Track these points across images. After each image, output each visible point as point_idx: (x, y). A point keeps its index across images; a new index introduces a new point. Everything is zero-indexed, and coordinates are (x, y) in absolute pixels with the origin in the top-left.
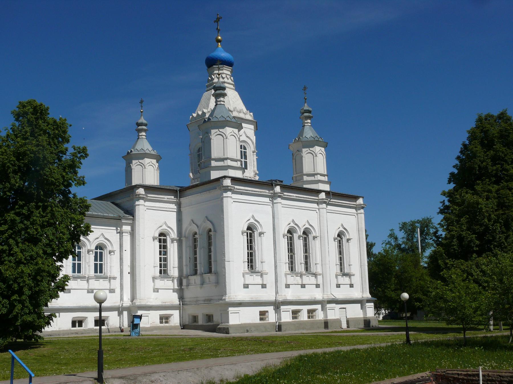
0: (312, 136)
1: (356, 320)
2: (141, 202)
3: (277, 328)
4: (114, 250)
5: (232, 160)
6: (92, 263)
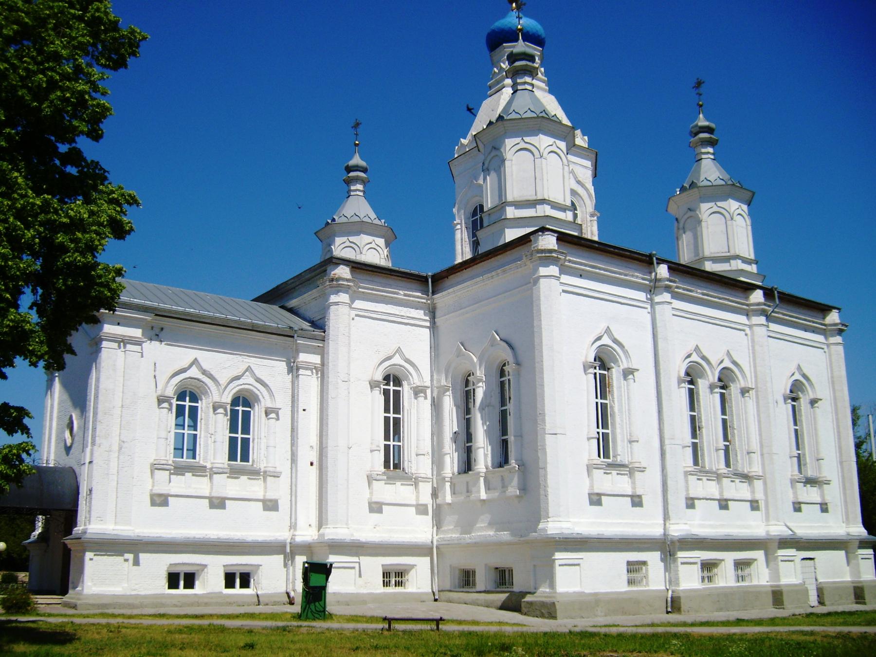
0: (721, 177)
1: (838, 588)
2: (344, 297)
3: (669, 604)
5: (555, 206)
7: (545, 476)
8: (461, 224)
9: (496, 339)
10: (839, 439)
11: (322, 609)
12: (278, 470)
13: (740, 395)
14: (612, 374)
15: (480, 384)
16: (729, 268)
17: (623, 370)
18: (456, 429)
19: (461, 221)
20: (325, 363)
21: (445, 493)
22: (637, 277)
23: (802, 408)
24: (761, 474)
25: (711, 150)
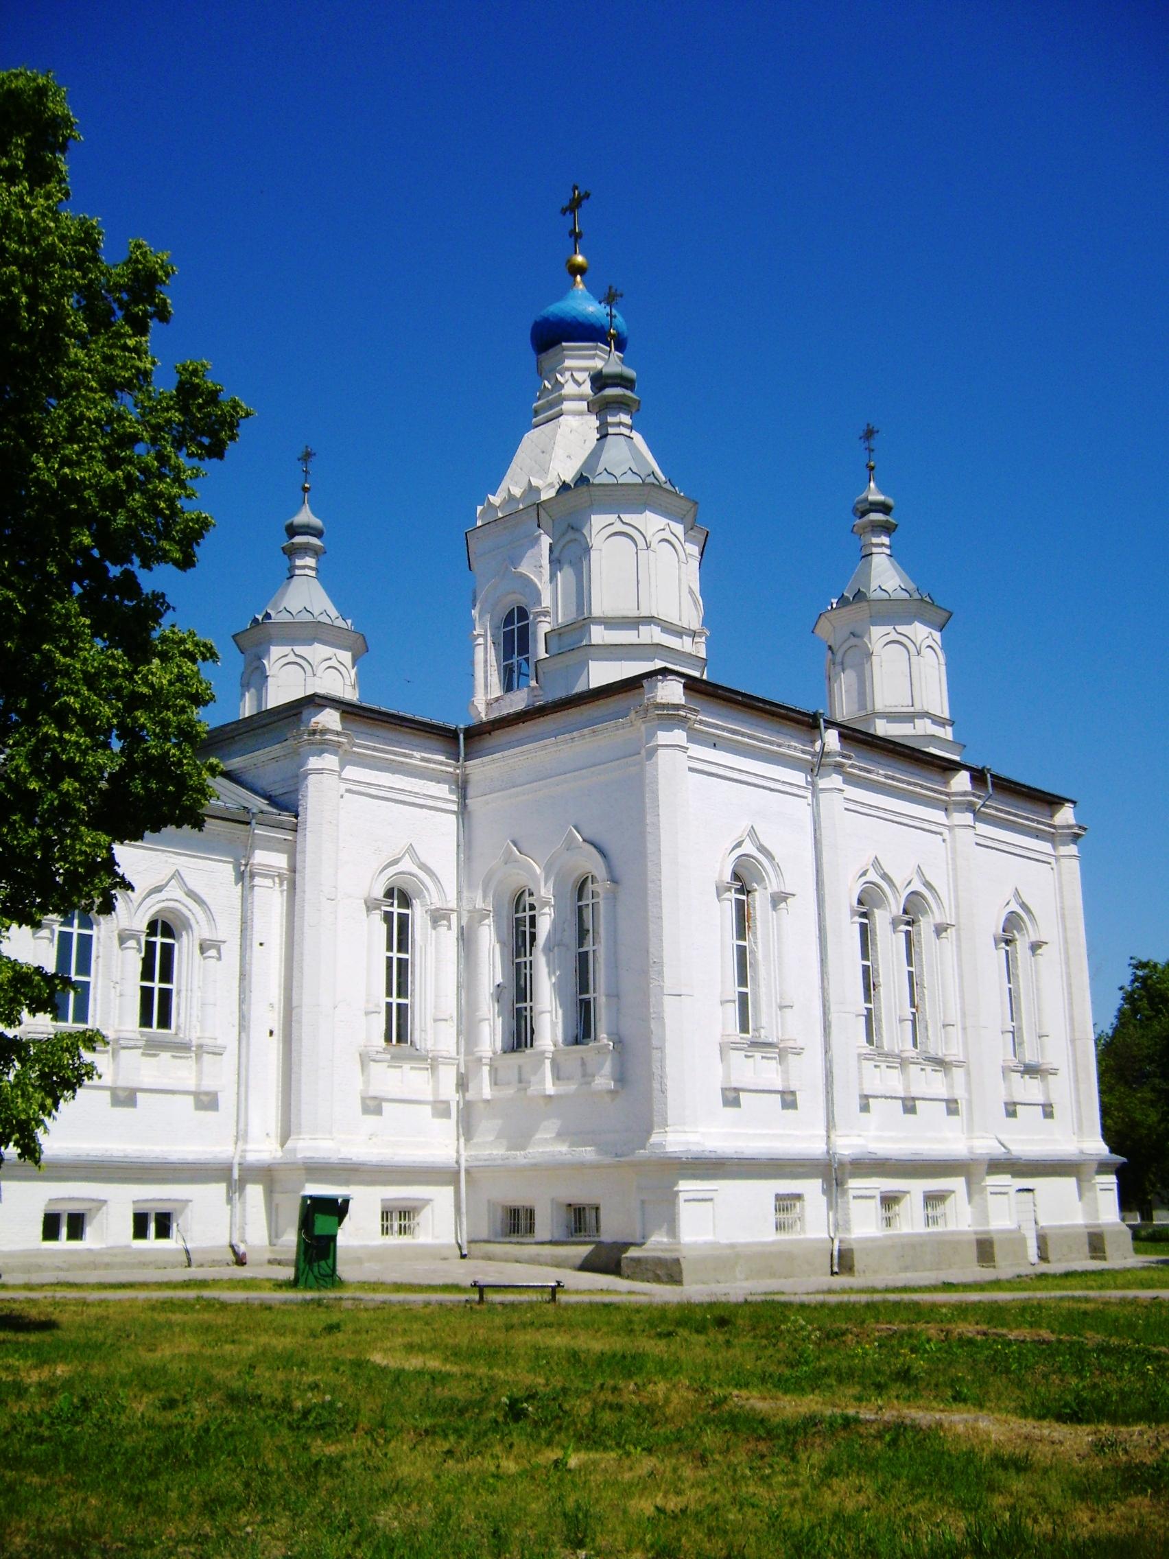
1: (1066, 1234)
2: (329, 761)
3: (836, 1261)
4: (221, 936)
6: (134, 984)
7: (662, 1061)
8: (485, 636)
9: (575, 837)
10: (1071, 1004)
11: (330, 1272)
12: (219, 1042)
13: (933, 935)
14: (754, 901)
15: (546, 910)
16: (913, 732)
17: (772, 896)
18: (499, 980)
19: (486, 631)
20: (298, 868)
21: (481, 1082)
22: (795, 748)
23: (1018, 956)
24: (961, 1059)
25: (885, 540)
